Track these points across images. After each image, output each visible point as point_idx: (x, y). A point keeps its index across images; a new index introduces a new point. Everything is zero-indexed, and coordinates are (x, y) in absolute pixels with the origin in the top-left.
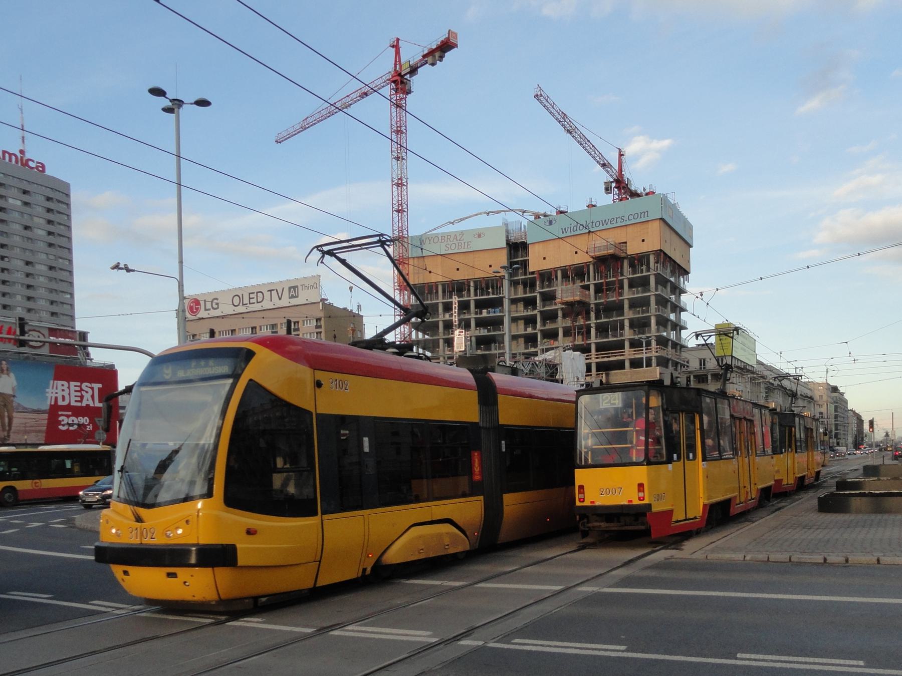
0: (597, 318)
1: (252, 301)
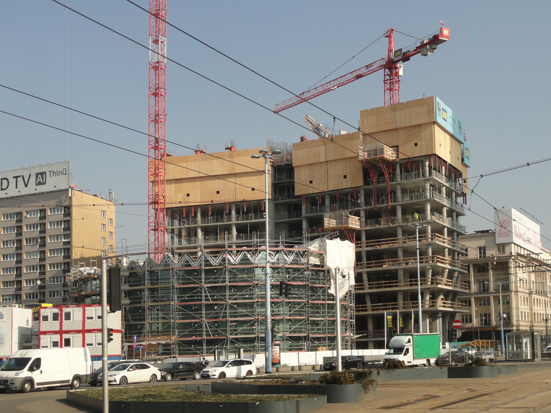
0: (367, 203)
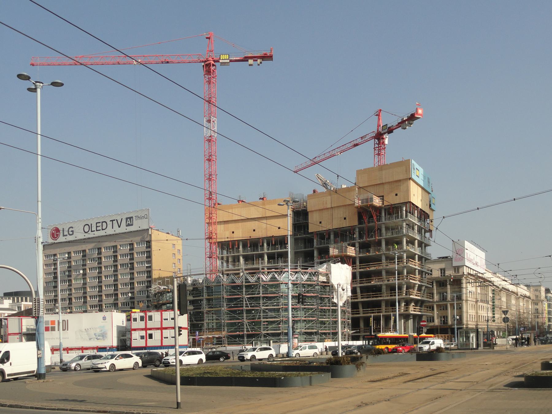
1: (98, 229)
